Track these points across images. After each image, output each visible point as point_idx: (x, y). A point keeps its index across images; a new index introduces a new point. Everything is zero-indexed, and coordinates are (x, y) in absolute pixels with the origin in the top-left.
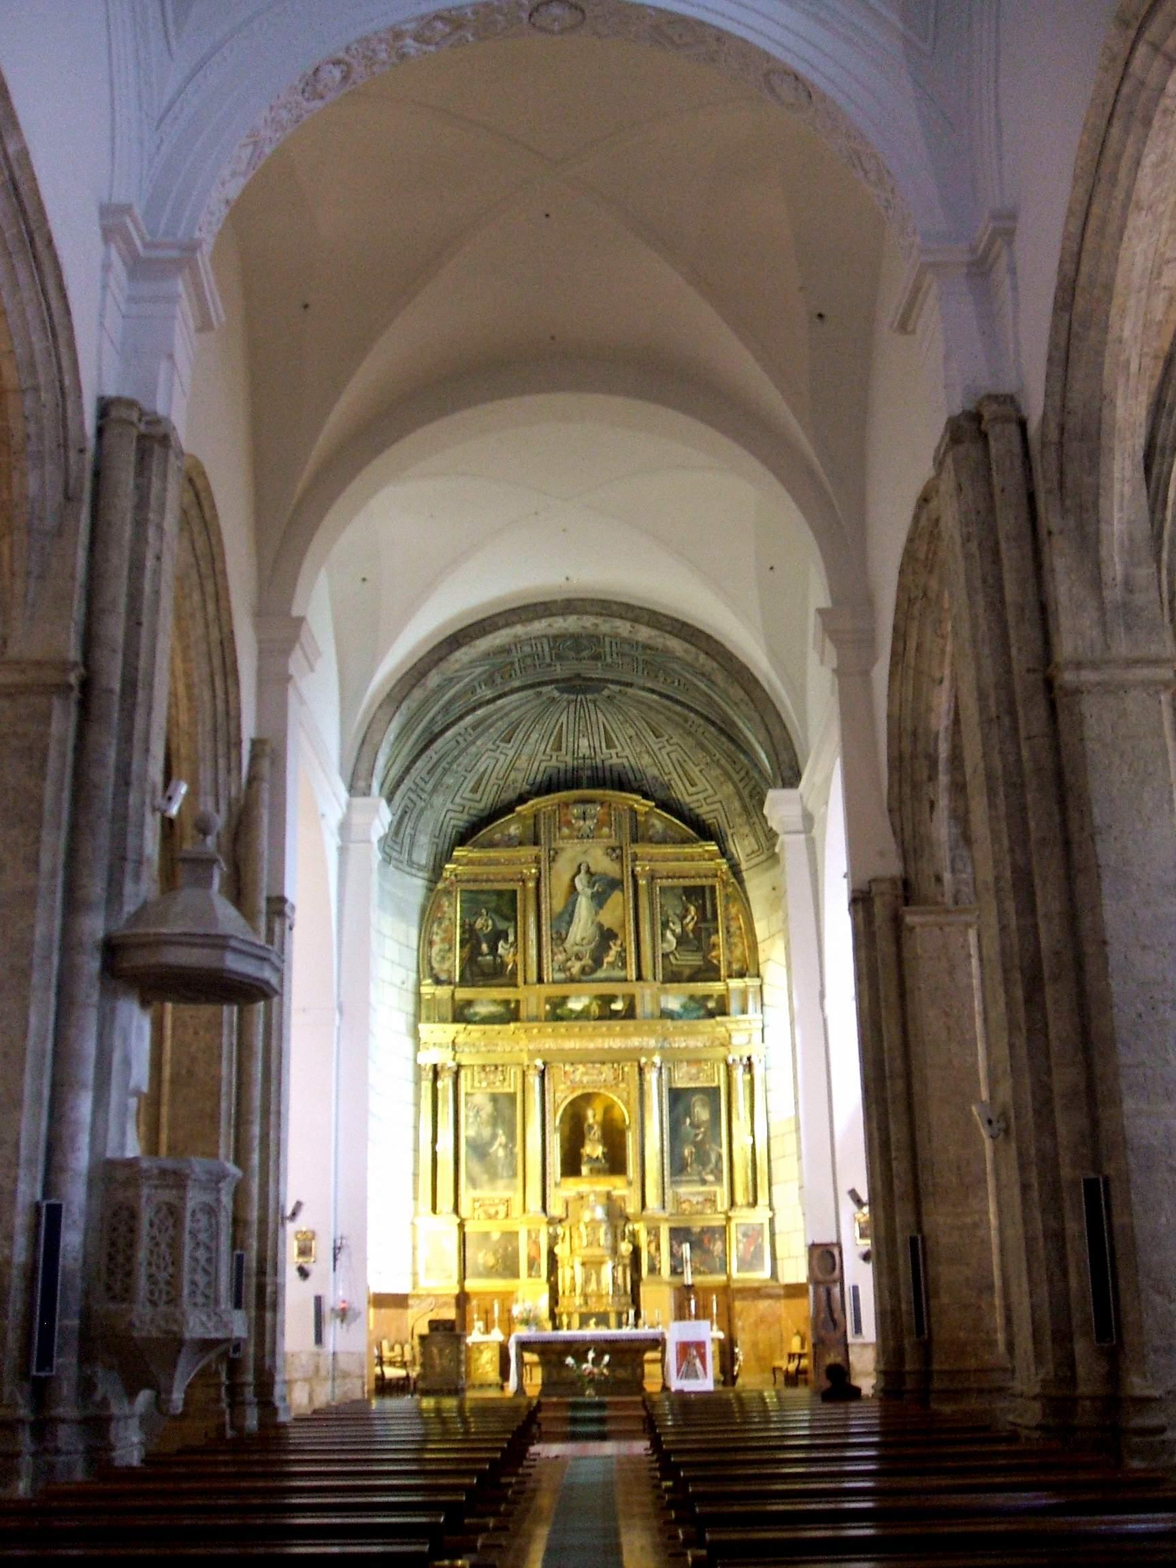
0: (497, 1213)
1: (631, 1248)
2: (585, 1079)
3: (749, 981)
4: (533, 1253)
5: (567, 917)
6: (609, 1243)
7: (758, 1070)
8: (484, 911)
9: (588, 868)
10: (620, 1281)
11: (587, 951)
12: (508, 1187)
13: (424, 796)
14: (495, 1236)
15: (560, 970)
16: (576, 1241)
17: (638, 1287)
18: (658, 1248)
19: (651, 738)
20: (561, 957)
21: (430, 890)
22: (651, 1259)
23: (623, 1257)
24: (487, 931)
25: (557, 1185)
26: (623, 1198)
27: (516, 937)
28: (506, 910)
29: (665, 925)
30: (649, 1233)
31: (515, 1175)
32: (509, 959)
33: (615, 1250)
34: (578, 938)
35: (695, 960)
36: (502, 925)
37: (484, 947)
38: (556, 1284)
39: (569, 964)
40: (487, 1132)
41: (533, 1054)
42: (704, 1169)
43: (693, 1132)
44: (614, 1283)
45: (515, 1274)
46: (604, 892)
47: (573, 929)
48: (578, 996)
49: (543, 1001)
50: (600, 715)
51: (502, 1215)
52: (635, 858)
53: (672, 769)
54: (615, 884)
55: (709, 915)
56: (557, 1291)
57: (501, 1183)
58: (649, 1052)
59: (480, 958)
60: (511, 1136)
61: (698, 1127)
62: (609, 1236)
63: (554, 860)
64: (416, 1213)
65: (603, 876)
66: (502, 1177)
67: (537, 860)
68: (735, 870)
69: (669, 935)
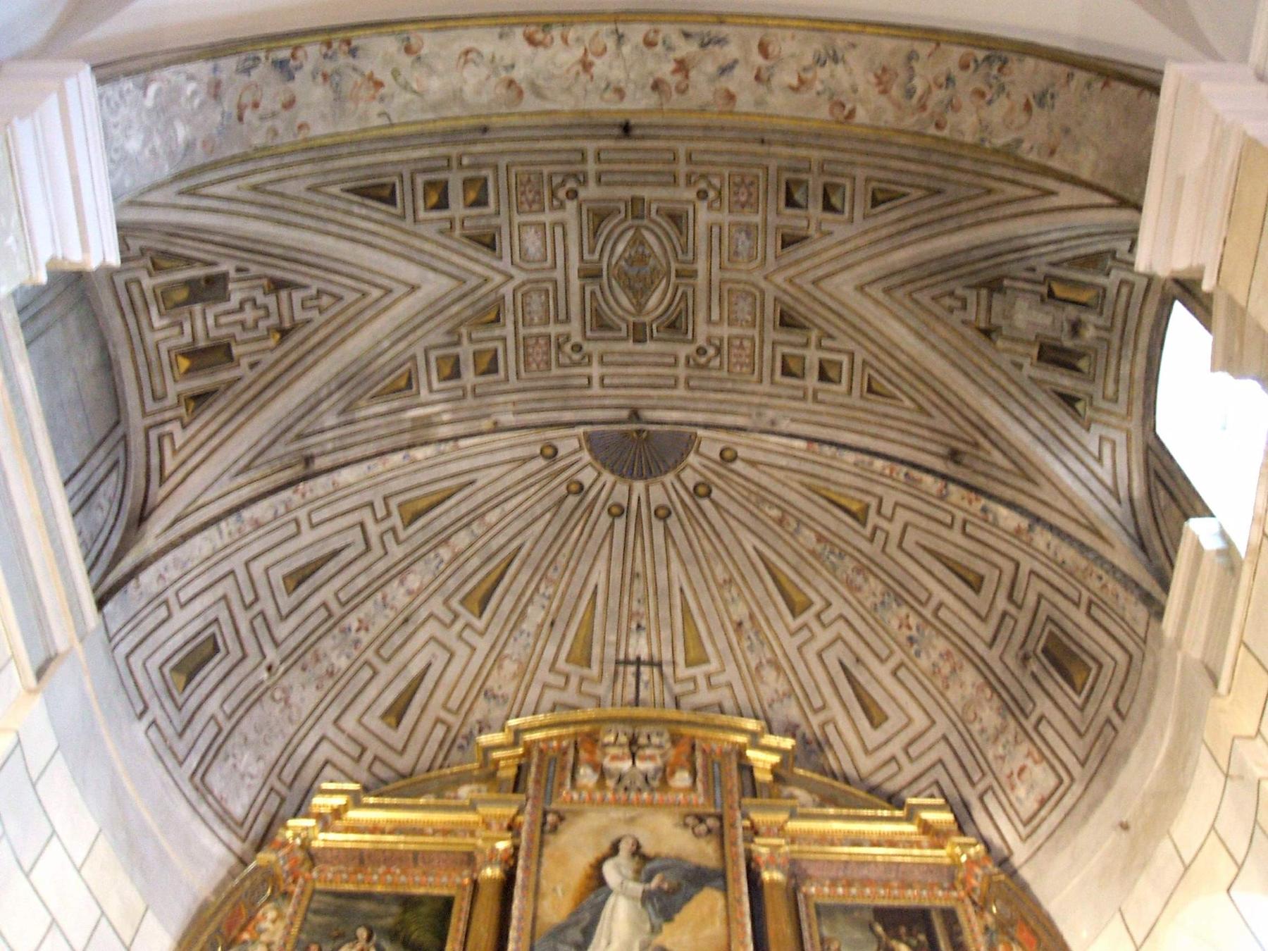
8: (362, 933)
13: (272, 655)
19: (780, 621)
46: (673, 891)
50: (675, 566)
53: (827, 690)
54: (699, 878)
63: (555, 829)
65: (674, 864)
67: (513, 827)
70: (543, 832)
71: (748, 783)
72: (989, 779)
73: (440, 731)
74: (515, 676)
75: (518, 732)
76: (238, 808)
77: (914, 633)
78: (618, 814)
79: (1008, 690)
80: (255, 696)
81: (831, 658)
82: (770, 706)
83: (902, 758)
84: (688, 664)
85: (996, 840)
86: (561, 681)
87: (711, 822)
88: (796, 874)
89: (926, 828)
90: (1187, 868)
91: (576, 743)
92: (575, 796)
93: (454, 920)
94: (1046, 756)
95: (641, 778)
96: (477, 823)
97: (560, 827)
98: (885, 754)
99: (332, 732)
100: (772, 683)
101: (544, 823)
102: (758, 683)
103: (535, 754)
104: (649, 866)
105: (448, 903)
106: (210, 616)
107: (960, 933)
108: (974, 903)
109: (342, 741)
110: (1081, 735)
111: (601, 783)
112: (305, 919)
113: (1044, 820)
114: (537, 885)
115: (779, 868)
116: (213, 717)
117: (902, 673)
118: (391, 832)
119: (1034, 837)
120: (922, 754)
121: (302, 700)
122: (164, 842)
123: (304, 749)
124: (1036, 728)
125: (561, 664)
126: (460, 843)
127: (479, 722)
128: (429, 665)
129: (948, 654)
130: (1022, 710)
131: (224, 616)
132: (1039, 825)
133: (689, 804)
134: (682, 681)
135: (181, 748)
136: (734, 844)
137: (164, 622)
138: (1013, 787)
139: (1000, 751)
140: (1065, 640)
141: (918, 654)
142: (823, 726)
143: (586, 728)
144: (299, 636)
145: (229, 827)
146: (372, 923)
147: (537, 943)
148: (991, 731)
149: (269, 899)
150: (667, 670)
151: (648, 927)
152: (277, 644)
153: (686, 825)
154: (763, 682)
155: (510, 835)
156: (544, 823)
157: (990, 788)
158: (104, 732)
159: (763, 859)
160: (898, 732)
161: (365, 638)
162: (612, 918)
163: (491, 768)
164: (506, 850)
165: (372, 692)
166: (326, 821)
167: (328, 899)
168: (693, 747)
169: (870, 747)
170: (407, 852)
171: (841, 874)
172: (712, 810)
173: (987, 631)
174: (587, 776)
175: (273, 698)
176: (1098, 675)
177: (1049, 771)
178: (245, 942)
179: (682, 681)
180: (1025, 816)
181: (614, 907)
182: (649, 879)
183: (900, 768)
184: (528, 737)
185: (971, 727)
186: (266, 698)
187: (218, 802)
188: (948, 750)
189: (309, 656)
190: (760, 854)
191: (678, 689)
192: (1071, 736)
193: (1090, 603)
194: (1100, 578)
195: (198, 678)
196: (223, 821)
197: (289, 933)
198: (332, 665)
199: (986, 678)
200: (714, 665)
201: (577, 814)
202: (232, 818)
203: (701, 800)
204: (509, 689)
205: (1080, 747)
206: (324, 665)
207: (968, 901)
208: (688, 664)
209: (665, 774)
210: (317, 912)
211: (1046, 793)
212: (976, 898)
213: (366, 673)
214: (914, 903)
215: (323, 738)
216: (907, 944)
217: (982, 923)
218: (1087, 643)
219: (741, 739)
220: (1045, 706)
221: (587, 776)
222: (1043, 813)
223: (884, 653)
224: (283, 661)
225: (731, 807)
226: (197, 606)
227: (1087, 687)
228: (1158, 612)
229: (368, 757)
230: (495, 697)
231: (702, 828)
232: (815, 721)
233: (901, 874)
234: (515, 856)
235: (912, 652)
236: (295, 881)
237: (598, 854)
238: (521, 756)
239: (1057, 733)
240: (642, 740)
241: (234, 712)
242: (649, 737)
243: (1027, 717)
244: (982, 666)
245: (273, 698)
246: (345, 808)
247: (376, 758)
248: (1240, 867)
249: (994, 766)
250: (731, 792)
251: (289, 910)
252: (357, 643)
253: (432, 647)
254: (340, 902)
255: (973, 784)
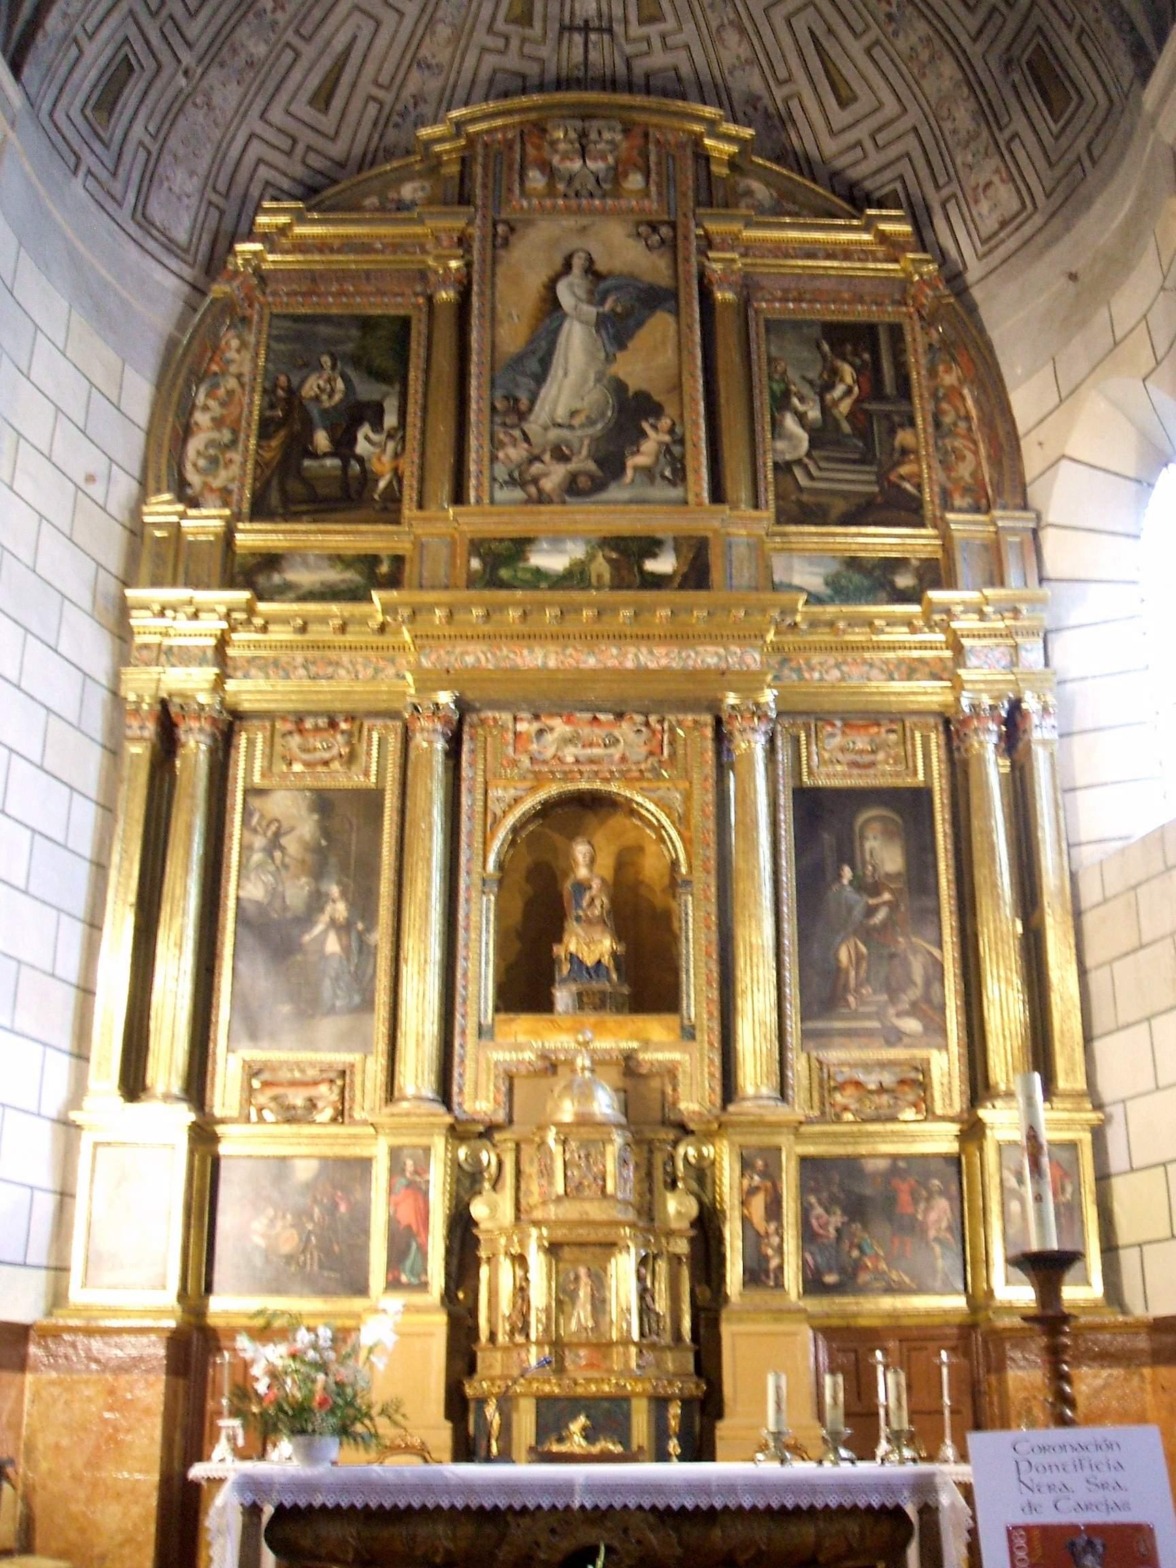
0: (312, 1104)
1: (693, 1209)
2: (570, 753)
3: (1005, 518)
4: (407, 1216)
5: (533, 365)
6: (629, 1192)
7: (1040, 732)
8: (326, 360)
9: (591, 260)
10: (661, 1305)
11: (582, 440)
12: (343, 1042)
13: (187, 58)
14: (304, 1171)
15: (512, 482)
16: (534, 1189)
17: (714, 1324)
18: (774, 1210)
20: (515, 453)
21: (199, 290)
22: (753, 1239)
23: (670, 1234)
24: (327, 403)
25: (481, 1031)
26: (670, 1072)
27: (402, 414)
28: (384, 362)
29: (781, 402)
30: (746, 1165)
31: (368, 1005)
32: (383, 466)
33: (648, 1211)
34: (561, 414)
35: (860, 481)
36: (367, 391)
37: (322, 439)
38: (473, 1312)
39: (536, 468)
40: (297, 891)
41: (426, 683)
42: (893, 1000)
43: (860, 902)
44: (645, 1310)
45: (360, 1288)
46: (628, 314)
47: (549, 392)
48: (557, 540)
49: (462, 550)
51: (327, 1114)
52: (708, 243)
55: (889, 387)
56: (474, 1331)
57: (328, 1027)
58: (749, 682)
59: (307, 463)
60: (364, 904)
61: (875, 890)
62: (630, 1172)
63: (506, 243)
64: (77, 1096)
66: (332, 1010)
67: (463, 242)
68: (955, 279)
69: (790, 422)
70: (494, 246)
71: (703, 174)
72: (954, 187)
73: (373, 108)
74: (449, 41)
75: (459, 125)
76: (181, 235)
77: (894, 9)
78: (570, 222)
79: (985, 92)
80: (177, 106)
81: (800, 24)
82: (731, 73)
83: (868, 145)
84: (641, 22)
85: (953, 252)
86: (501, 43)
87: (665, 231)
88: (748, 288)
89: (883, 238)
90: (1116, 344)
91: (522, 133)
92: (525, 204)
93: (414, 345)
94: (1014, 176)
95: (592, 179)
96: (426, 236)
97: (513, 239)
98: (850, 137)
99: (259, 128)
100: (733, 48)
101: (495, 235)
102: (720, 48)
103: (480, 149)
104: (603, 285)
105: (405, 322)
106: (119, 37)
107: (904, 351)
108: (922, 318)
109: (270, 134)
110: (1051, 165)
111: (551, 185)
112: (268, 347)
113: (1003, 241)
114: (493, 309)
115: (731, 286)
116: (141, 143)
117: (877, 52)
118: (340, 251)
119: (990, 258)
120: (890, 143)
121: (225, 99)
122: (125, 294)
123: (234, 152)
124: (1008, 144)
125: (500, 25)
126: (408, 261)
127: (414, 97)
128: (354, 38)
129: (929, 40)
130: (998, 123)
131: (133, 32)
132: (996, 246)
133: (642, 211)
134: (635, 40)
135: (117, 187)
136: (687, 260)
137: (77, 60)
138: (976, 202)
139: (970, 158)
140: (1050, 57)
141: (896, 34)
142: (786, 101)
143: (533, 116)
144: (212, 30)
145: (177, 256)
146: (333, 349)
147: (497, 374)
148: (963, 134)
149: (229, 328)
150: (618, 28)
151: (602, 355)
152: (189, 45)
153: (639, 235)
154: (725, 47)
155: (460, 252)
156: (495, 235)
157: (954, 196)
158: (50, 206)
159: (714, 278)
160: (866, 116)
161: (281, 17)
162: (567, 340)
163: (434, 162)
164: (458, 269)
165: (296, 75)
166: (270, 240)
167: (288, 324)
168: (646, 135)
169: (835, 127)
170: (357, 271)
171: (793, 285)
172: (666, 217)
173: (973, 23)
174: (536, 179)
175: (195, 105)
176: (1078, 108)
177: (1014, 194)
178: (215, 374)
179: (635, 40)
180: (984, 235)
181: (570, 331)
182: (602, 302)
183: (865, 157)
184: (472, 129)
185: (943, 124)
186: (189, 105)
187: (163, 234)
188: (916, 144)
189: (225, 50)
190: (715, 271)
191: (629, 49)
192: (1041, 164)
193: (1082, 31)
194: (1096, 10)
195: (118, 108)
196: (169, 250)
197: (256, 365)
198: (252, 55)
199: (965, 74)
200: (670, 24)
201: (529, 223)
202: (179, 246)
203: (655, 206)
204: (444, 56)
205: (1049, 176)
206: (243, 55)
207: (916, 317)
208: (641, 22)
209: (617, 174)
210: (278, 338)
211: (1007, 215)
212: (924, 313)
213: (288, 56)
214: (863, 318)
215: (252, 136)
216: (852, 365)
217: (927, 340)
218: (1073, 72)
219: (698, 128)
220: (1019, 124)
221: (536, 179)
222: (1002, 235)
223: (859, 27)
224: (200, 60)
225: (685, 215)
226: (105, 32)
227: (1066, 116)
228: (1144, 74)
229: (300, 148)
230: (429, 67)
231: (655, 238)
232: (779, 93)
233: (856, 290)
234: (469, 275)
235: (890, 30)
236: (251, 306)
237: (551, 273)
238: (464, 148)
239: (1027, 153)
240: (593, 136)
241: (158, 131)
242: (600, 133)
243: (1001, 129)
244: (963, 61)
245: (195, 105)
246: (288, 226)
247: (309, 148)
248: (1158, 363)
249: (961, 174)
250: (685, 195)
251: (252, 339)
252: (274, 24)
253: (357, 17)
254: (301, 326)
255: (937, 187)
